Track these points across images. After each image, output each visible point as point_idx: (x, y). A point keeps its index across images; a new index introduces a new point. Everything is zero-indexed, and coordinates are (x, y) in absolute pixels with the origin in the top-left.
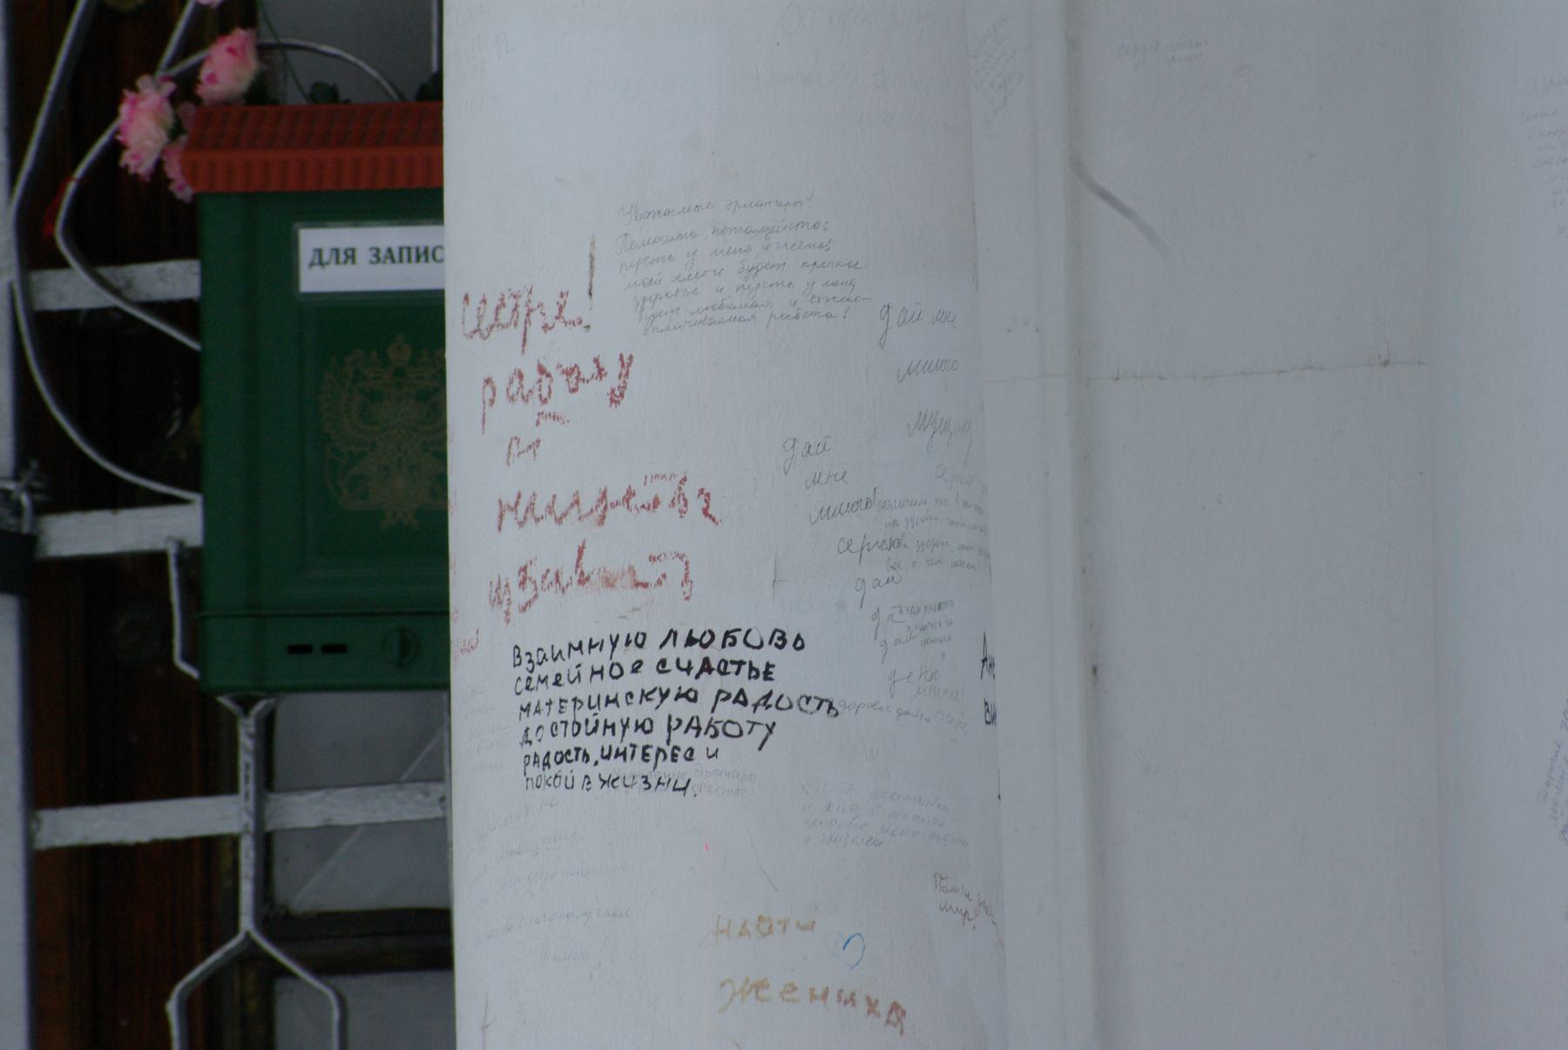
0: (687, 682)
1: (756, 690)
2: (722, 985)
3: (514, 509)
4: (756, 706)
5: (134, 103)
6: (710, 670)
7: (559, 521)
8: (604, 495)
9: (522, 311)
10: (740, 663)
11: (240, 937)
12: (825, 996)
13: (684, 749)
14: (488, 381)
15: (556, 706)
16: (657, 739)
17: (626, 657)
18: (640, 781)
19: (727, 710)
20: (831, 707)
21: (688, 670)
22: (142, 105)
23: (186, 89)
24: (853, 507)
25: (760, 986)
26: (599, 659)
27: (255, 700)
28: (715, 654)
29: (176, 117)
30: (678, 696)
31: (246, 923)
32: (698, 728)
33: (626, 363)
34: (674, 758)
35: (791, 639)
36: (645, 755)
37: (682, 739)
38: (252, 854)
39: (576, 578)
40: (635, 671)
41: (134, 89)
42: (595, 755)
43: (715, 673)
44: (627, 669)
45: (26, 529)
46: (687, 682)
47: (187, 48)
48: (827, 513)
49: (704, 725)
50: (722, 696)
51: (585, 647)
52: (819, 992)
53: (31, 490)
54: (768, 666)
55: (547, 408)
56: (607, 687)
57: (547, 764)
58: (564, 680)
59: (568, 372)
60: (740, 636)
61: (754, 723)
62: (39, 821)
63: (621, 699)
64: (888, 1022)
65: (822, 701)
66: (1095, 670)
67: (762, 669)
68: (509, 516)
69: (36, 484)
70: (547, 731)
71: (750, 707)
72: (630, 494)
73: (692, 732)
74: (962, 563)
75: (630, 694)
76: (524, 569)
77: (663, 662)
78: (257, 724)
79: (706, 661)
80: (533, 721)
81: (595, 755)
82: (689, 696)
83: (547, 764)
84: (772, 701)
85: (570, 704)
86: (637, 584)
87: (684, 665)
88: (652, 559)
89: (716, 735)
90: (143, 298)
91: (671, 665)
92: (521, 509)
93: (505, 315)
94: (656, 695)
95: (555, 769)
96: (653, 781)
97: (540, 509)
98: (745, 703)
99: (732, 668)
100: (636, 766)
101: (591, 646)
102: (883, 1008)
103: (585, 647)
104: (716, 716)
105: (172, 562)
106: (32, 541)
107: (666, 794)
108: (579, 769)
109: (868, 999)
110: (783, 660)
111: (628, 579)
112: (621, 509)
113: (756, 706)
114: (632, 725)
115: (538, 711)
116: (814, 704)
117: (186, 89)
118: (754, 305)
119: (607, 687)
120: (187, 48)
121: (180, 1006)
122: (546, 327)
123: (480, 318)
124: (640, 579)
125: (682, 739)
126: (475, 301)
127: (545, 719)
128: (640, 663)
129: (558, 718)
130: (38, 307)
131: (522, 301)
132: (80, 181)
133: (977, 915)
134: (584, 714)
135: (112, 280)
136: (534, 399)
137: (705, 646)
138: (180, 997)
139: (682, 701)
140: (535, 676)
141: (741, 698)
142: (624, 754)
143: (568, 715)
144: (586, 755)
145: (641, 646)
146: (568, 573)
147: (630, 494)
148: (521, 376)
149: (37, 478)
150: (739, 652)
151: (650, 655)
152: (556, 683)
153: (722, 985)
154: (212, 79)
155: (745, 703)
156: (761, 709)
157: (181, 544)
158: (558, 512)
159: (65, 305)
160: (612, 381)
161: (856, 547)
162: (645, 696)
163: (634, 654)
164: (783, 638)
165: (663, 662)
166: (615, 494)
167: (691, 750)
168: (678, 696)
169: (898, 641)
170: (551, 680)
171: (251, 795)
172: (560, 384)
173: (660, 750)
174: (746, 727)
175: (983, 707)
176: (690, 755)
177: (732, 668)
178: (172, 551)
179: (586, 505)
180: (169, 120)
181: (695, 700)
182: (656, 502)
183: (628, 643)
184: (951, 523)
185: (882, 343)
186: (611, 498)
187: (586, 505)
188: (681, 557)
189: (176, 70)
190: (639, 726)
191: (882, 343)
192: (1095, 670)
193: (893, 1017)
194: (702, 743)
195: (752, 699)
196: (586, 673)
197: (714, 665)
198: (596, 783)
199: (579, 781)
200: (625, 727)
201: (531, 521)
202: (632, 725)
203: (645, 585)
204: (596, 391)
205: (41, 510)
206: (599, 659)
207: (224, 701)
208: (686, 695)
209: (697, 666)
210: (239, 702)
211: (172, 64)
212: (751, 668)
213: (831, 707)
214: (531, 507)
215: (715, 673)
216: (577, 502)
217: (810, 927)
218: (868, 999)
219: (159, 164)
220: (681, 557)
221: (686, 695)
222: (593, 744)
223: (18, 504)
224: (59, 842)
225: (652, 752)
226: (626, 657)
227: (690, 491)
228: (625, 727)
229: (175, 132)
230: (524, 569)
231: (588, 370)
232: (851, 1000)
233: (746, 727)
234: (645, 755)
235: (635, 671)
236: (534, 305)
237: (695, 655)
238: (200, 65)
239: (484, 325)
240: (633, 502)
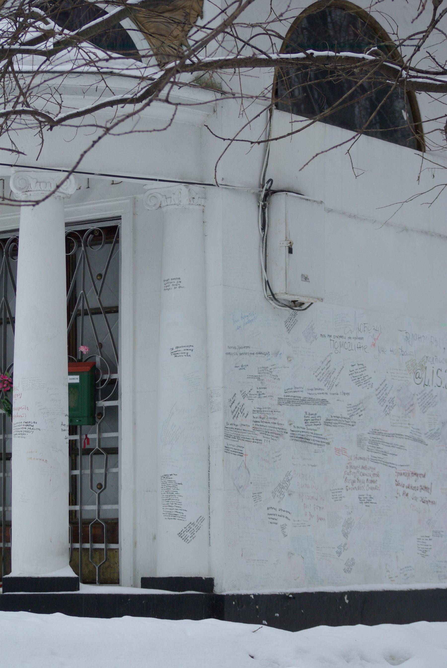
0: (25, 427)
1: (32, 428)
16: (22, 433)
17: (20, 424)
19: (29, 430)
25: (31, 458)
26: (18, 424)
28: (28, 424)
33: (21, 394)
46: (25, 427)
48: (40, 409)
50: (28, 428)
82: (25, 428)
100: (21, 436)
102: (45, 460)
108: (17, 436)
110: (35, 425)
125: (25, 433)
141: (30, 429)
150: (30, 424)
151: (22, 424)
160: (20, 396)
166: (20, 407)
185: (47, 392)
191: (47, 392)
194: (26, 433)
204: (19, 397)
206: (18, 424)
222: (18, 433)
227: (26, 407)
232: (41, 460)
237: (26, 424)
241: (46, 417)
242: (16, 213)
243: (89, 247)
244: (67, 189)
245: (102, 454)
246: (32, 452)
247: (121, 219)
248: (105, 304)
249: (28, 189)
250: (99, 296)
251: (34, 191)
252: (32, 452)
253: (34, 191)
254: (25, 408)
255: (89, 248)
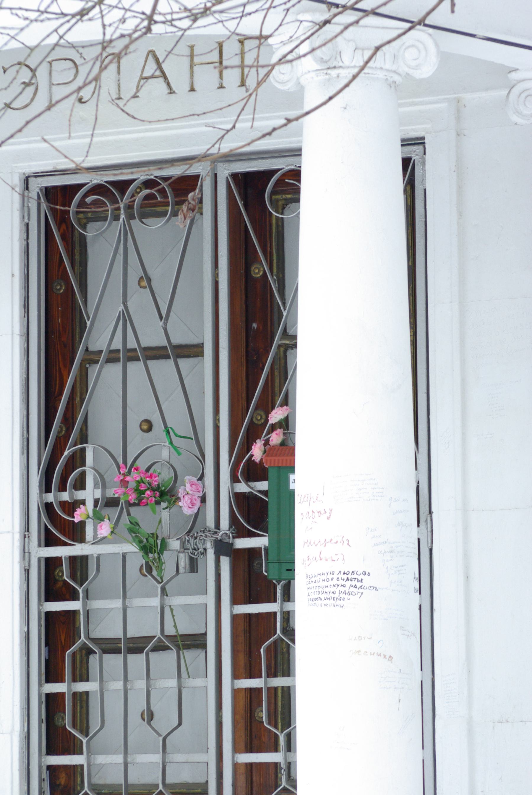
0: (343, 583)
1: (359, 584)
2: (350, 651)
3: (306, 543)
4: (359, 588)
5: (255, 445)
6: (348, 580)
7: (316, 546)
8: (326, 540)
9: (309, 498)
10: (355, 579)
11: (277, 635)
12: (374, 654)
13: (342, 598)
14: (302, 514)
15: (315, 588)
16: (337, 595)
17: (330, 577)
18: (333, 605)
19: (352, 589)
20: (376, 589)
21: (344, 580)
22: (256, 446)
23: (267, 443)
24: (383, 543)
25: (358, 652)
26: (324, 577)
27: (281, 582)
28: (350, 576)
29: (265, 449)
30: (341, 586)
31: (278, 632)
32: (346, 593)
33: (331, 510)
34: (340, 600)
35: (367, 573)
36: (334, 599)
37: (342, 596)
38: (280, 616)
39: (319, 559)
40: (332, 580)
41: (256, 443)
42: (323, 599)
43: (350, 581)
44: (330, 579)
45: (231, 542)
46: (343, 583)
47: (268, 433)
48: (376, 545)
49: (347, 593)
50: (351, 586)
51: (321, 574)
52: (372, 653)
53: (232, 533)
54: (362, 579)
55: (314, 520)
56: (326, 583)
57: (313, 601)
58: (316, 582)
59: (318, 512)
60: (355, 572)
61: (358, 592)
62: (234, 608)
63: (329, 586)
64: (389, 660)
65: (374, 587)
66: (467, 577)
67: (360, 580)
68: (306, 544)
69: (233, 532)
70: (313, 593)
71: (357, 589)
72: (331, 540)
73: (344, 594)
74: (409, 556)
75: (331, 585)
76: (308, 557)
77: (338, 578)
78: (281, 586)
79: (348, 578)
80: (310, 591)
81: (323, 599)
82: (343, 586)
83: (313, 601)
84: (362, 587)
85: (318, 587)
86: (333, 560)
87: (343, 579)
88: (336, 555)
89: (349, 595)
90: (258, 490)
91: (340, 579)
92: (308, 543)
93: (306, 498)
94: (336, 586)
95: (314, 602)
96: (335, 605)
97: (312, 543)
98: (356, 588)
99: (353, 580)
100: (332, 602)
101: (323, 574)
102: (387, 657)
103: (321, 574)
104: (350, 590)
105: (263, 550)
106: (232, 544)
107: (338, 608)
108: (319, 602)
109: (384, 655)
110: (365, 578)
111: (330, 559)
112: (329, 543)
113: (359, 588)
114: (331, 592)
115: (311, 589)
116: (372, 588)
117: (267, 443)
118: (360, 497)
119: (326, 583)
120: (268, 433)
121: (263, 650)
122: (314, 502)
123: (301, 499)
124: (333, 559)
125: (342, 596)
126: (300, 495)
127: (313, 590)
128: (333, 578)
129: (316, 590)
130: (235, 491)
131: (309, 496)
132: (244, 463)
133: (411, 636)
134: (321, 590)
135: (251, 486)
136: (311, 518)
137: (347, 575)
138: (263, 649)
139: (342, 587)
140: (310, 581)
141: (355, 587)
142: (329, 599)
143: (317, 590)
144: (321, 599)
145: (333, 574)
146: (318, 558)
147: (331, 540)
148: (308, 513)
149: (234, 530)
150: (355, 576)
151: (335, 576)
152: (315, 582)
153: (350, 651)
154: (272, 440)
155: (356, 588)
156: (360, 589)
157: (265, 546)
158: (316, 544)
159: (241, 491)
160: (328, 514)
161: (383, 552)
162: (334, 586)
163: (331, 576)
164: (365, 573)
165: (338, 578)
166: (328, 540)
167: (344, 598)
168: (341, 586)
169: (392, 574)
170: (314, 582)
171: (280, 603)
172: (317, 514)
173: (337, 598)
174: (356, 593)
175: (414, 589)
176: (344, 599)
177: (353, 580)
178: (263, 547)
179: (322, 543)
180: (263, 449)
181: (345, 587)
182: (337, 542)
183: (330, 574)
184: (406, 547)
185: (390, 506)
186: (327, 541)
187: (322, 543)
188: (342, 554)
189: (266, 438)
190: (333, 593)
191: (390, 506)
192: (467, 577)
193: (390, 659)
194: (347, 597)
195: (358, 587)
196: (321, 580)
197: (349, 579)
198: (323, 605)
199: (320, 605)
200: (330, 593)
201: (310, 545)
202: (331, 592)
203: (334, 561)
204: (324, 517)
205: (234, 537)
206: (324, 577)
207: (274, 581)
208: (343, 586)
209: (346, 579)
210: (277, 582)
211: (264, 437)
212: (358, 580)
213: (376, 589)
214: (310, 543)
215: (350, 581)
216: (320, 542)
217: (370, 638)
218: (384, 655)
219: (261, 459)
220: (342, 554)
221: (343, 586)
222: (323, 596)
223: (229, 536)
224: (238, 613)
225: (335, 598)
226: (330, 577)
227: (345, 539)
228: (330, 593)
229: (264, 452)
230: (308, 557)
231: (323, 512)
232: (380, 655)
233: (356, 593)
234: (334, 599)
235: (332, 580)
236: (311, 497)
237: (345, 577)
238: (270, 437)
239: (301, 501)
240: (332, 542)
241: (388, 561)
242: (126, 129)
243: (137, 219)
244: (417, 66)
245: (168, 648)
246: (360, 638)
247: (300, 155)
248: (176, 340)
249: (335, 64)
250: (166, 323)
251: (348, 67)
252: (360, 638)
253: (348, 67)
254: (342, 542)
255: (135, 223)
